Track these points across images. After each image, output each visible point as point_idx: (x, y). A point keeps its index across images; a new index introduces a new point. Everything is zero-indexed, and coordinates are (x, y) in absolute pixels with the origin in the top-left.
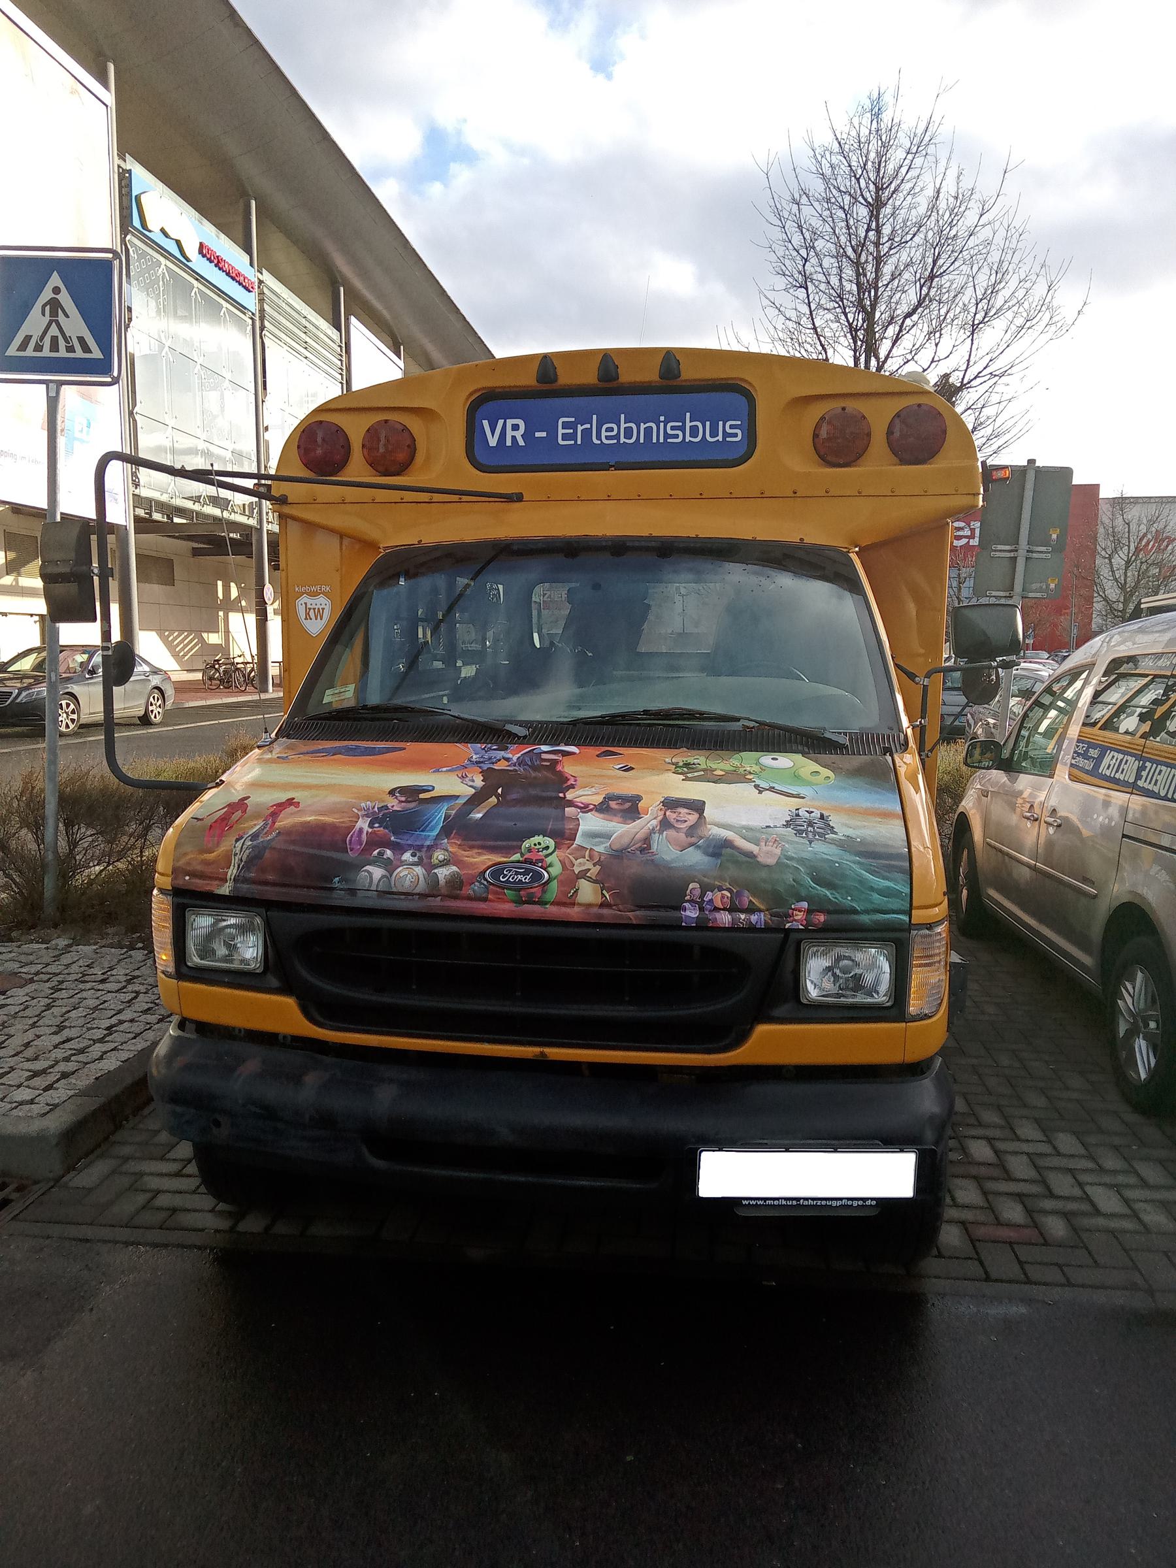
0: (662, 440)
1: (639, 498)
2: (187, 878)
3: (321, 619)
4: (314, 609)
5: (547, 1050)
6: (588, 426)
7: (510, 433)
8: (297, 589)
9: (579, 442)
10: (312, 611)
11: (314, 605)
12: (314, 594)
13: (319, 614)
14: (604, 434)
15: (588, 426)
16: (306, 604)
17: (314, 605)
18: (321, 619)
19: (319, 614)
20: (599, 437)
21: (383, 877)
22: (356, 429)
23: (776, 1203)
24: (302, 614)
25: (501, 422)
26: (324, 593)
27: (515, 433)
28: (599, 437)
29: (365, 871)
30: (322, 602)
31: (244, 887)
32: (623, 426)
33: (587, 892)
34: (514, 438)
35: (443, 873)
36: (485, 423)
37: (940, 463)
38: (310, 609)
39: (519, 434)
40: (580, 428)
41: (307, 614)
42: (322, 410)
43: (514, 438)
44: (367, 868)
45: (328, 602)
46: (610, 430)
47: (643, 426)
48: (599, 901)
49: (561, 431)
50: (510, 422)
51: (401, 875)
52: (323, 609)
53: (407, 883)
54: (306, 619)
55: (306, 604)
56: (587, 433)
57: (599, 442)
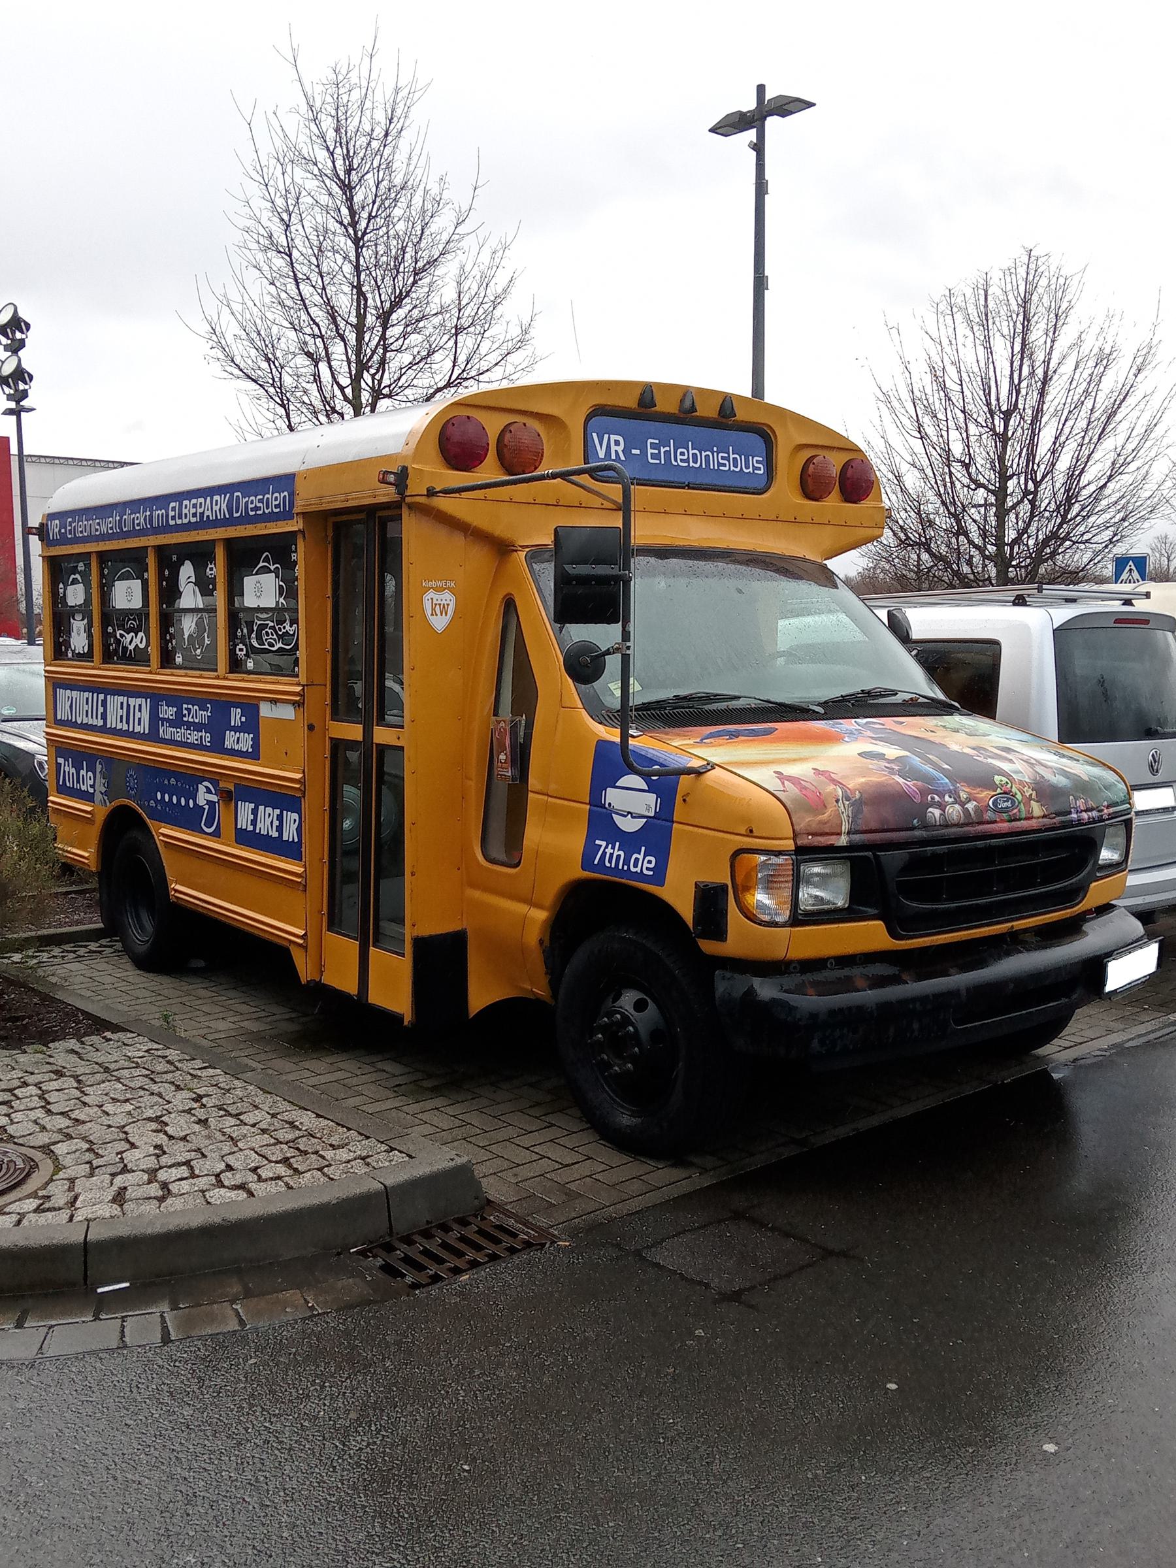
0: (716, 468)
1: (705, 515)
2: (810, 837)
3: (446, 615)
4: (440, 605)
5: (1015, 923)
6: (668, 449)
7: (613, 448)
8: (424, 584)
9: (663, 462)
10: (438, 606)
11: (439, 600)
12: (439, 590)
13: (444, 610)
14: (679, 457)
15: (668, 449)
16: (432, 599)
17: (439, 600)
18: (446, 615)
19: (444, 610)
20: (676, 461)
21: (941, 815)
22: (493, 425)
23: (1125, 988)
24: (429, 611)
25: (606, 436)
26: (448, 589)
27: (617, 448)
28: (676, 461)
29: (930, 812)
30: (447, 598)
31: (857, 838)
32: (691, 452)
33: (1037, 809)
34: (616, 452)
35: (970, 806)
36: (595, 435)
37: (867, 503)
38: (436, 604)
39: (620, 449)
40: (663, 450)
41: (433, 609)
42: (457, 404)
43: (616, 452)
44: (930, 810)
45: (453, 598)
46: (682, 454)
47: (704, 454)
48: (1042, 814)
49: (650, 451)
50: (613, 438)
51: (950, 812)
52: (448, 605)
53: (955, 818)
54: (432, 615)
55: (432, 599)
56: (667, 453)
57: (676, 464)
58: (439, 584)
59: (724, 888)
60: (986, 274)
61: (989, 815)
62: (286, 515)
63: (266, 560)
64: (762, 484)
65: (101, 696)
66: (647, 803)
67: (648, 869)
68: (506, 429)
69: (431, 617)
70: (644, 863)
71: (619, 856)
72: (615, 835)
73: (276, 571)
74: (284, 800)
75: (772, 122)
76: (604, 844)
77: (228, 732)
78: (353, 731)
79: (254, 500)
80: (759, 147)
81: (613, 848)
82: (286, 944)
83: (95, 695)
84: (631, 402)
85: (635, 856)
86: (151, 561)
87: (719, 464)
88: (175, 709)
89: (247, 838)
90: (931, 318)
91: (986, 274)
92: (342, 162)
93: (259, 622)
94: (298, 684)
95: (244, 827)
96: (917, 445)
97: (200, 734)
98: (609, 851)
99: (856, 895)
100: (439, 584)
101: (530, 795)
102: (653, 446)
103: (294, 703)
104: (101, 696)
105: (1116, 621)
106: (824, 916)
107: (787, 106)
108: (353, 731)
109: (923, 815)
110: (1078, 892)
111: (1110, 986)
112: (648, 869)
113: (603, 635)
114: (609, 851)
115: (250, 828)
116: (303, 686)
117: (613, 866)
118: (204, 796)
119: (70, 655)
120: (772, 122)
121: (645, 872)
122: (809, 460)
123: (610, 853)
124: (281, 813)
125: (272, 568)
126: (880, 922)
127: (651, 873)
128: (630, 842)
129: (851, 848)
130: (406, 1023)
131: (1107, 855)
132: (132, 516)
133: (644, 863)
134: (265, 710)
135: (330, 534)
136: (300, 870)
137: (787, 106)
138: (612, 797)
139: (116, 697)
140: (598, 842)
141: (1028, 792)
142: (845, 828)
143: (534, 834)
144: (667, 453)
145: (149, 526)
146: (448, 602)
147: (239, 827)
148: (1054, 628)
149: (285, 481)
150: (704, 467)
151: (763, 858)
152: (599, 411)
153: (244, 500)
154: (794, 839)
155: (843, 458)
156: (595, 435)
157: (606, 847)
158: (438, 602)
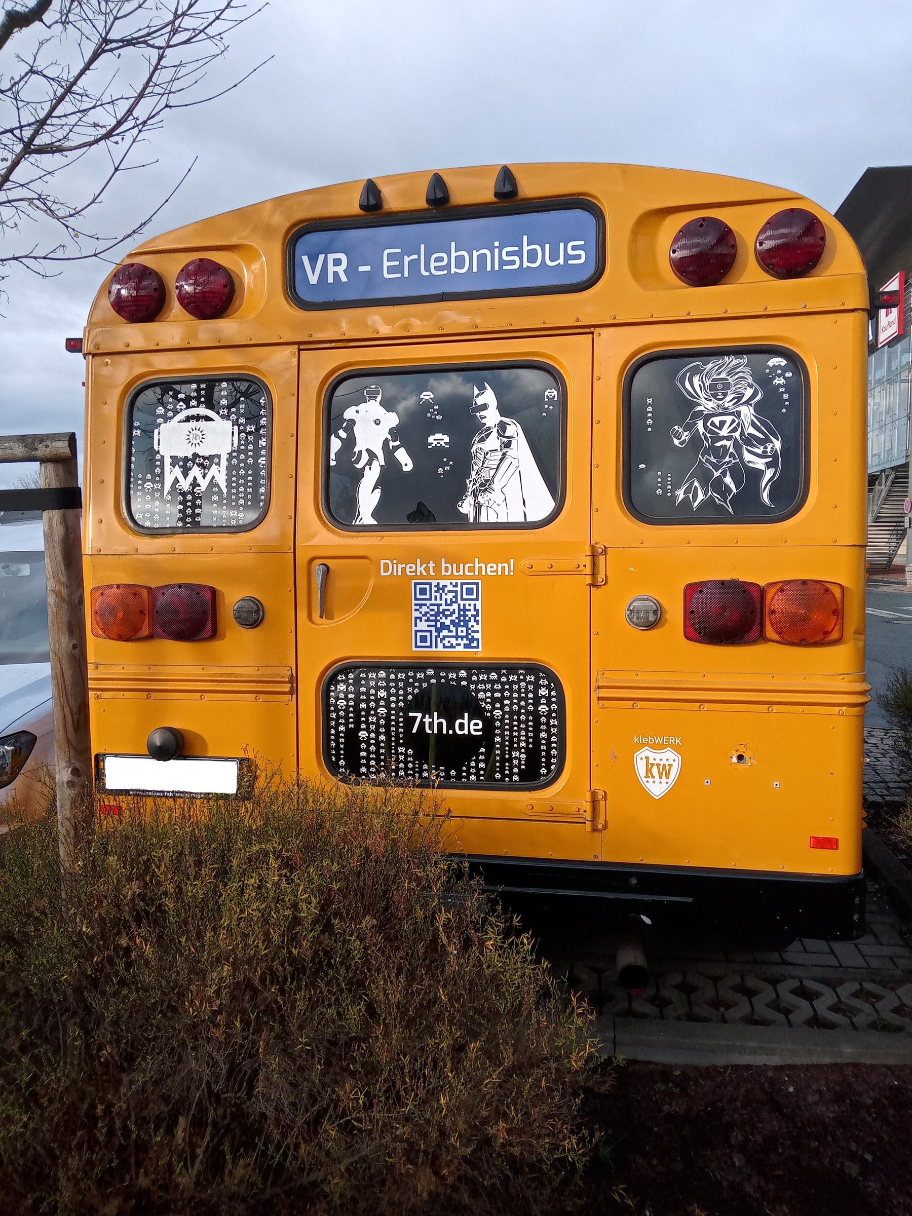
0: (497, 268)
6: (416, 257)
7: (331, 269)
13: (664, 771)
14: (433, 264)
15: (416, 257)
19: (664, 771)
26: (672, 746)
27: (337, 269)
28: (427, 268)
30: (669, 757)
36: (305, 259)
38: (652, 765)
39: (341, 269)
40: (407, 259)
43: (336, 274)
49: (386, 264)
50: (331, 257)
52: (670, 766)
55: (647, 758)
56: (414, 264)
57: (428, 274)
58: (658, 740)
67: (475, 730)
69: (645, 780)
71: (440, 724)
76: (419, 715)
81: (431, 717)
87: (502, 262)
98: (427, 720)
100: (658, 740)
102: (391, 257)
112: (475, 730)
117: (436, 732)
121: (473, 733)
127: (480, 733)
144: (414, 264)
146: (671, 762)
150: (475, 270)
156: (305, 259)
157: (423, 717)
158: (655, 762)
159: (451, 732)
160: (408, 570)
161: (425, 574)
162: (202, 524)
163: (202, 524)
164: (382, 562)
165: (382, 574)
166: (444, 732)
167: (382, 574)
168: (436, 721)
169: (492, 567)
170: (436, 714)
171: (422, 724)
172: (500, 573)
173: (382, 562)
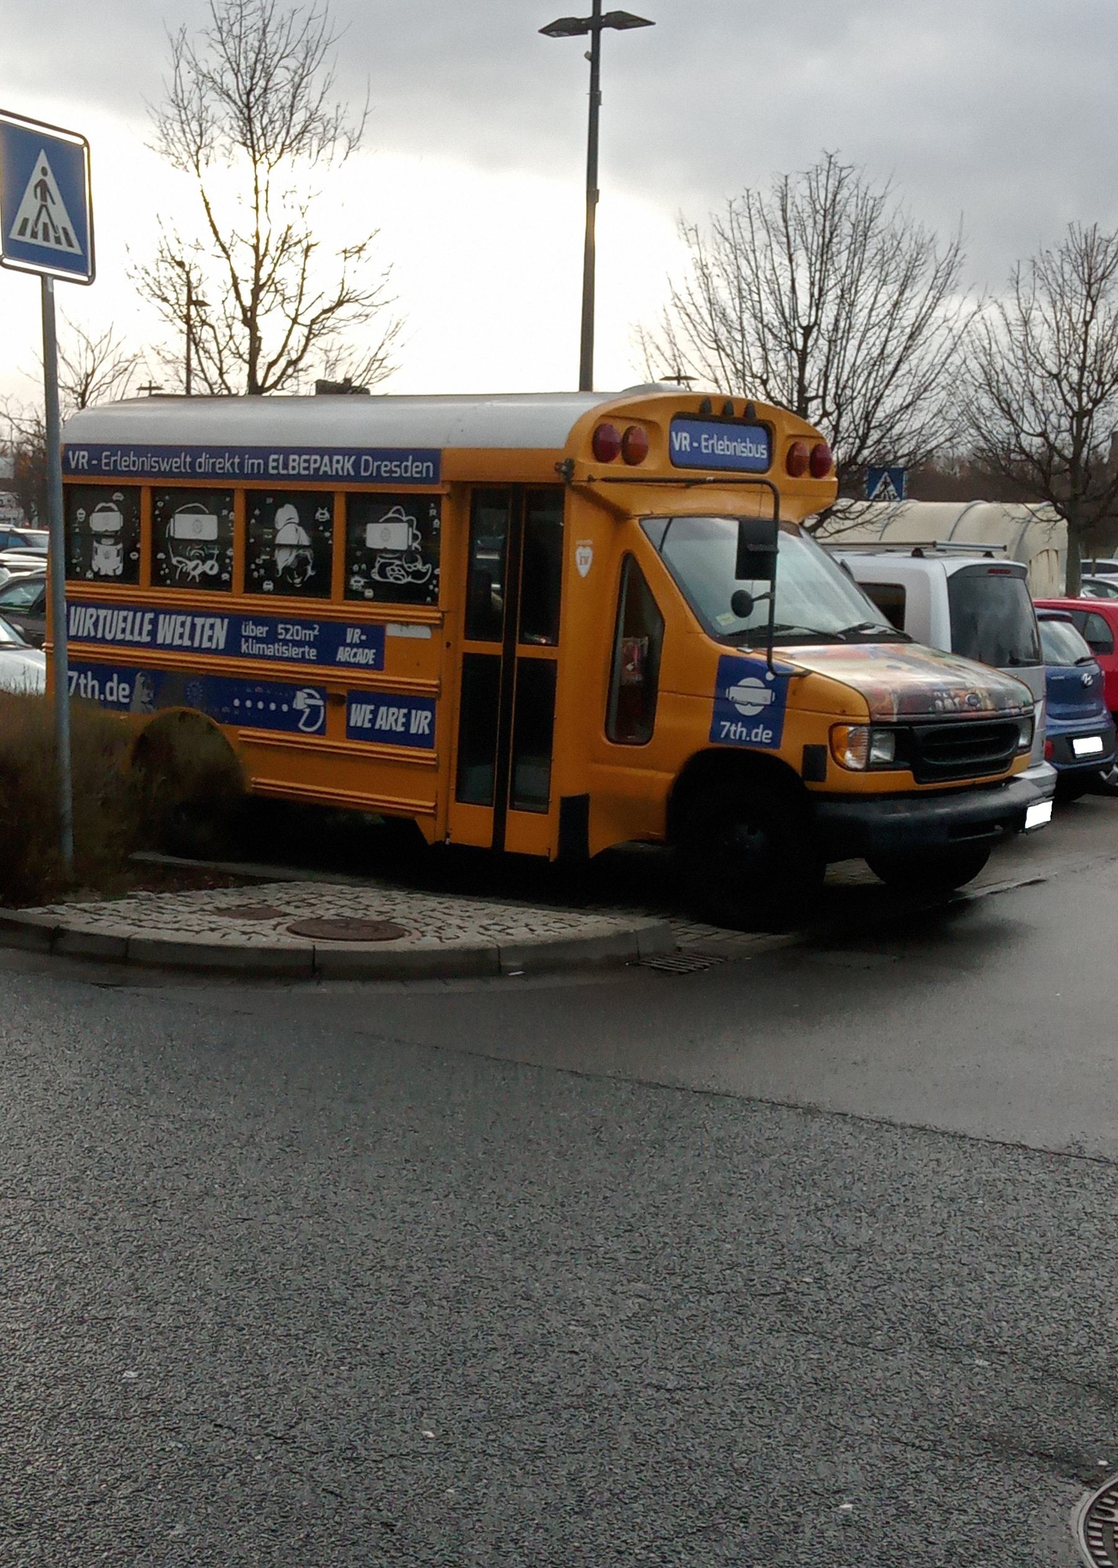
22: (620, 428)
24: (578, 561)
35: (957, 700)
59: (824, 748)
60: (786, 177)
61: (966, 707)
62: (435, 480)
63: (397, 511)
64: (763, 466)
65: (149, 616)
66: (765, 696)
68: (629, 431)
70: (762, 735)
71: (742, 732)
72: (736, 718)
73: (410, 523)
74: (422, 702)
75: (607, 33)
76: (728, 724)
77: (341, 649)
78: (494, 648)
79: (386, 466)
80: (594, 57)
82: (410, 815)
83: (139, 615)
84: (694, 409)
85: (755, 731)
86: (239, 501)
88: (266, 629)
89: (356, 733)
90: (724, 215)
91: (786, 177)
92: (272, 97)
93: (382, 561)
94: (439, 611)
95: (359, 724)
96: (713, 356)
97: (302, 650)
98: (82, 681)
99: (897, 756)
101: (660, 694)
103: (430, 625)
104: (149, 616)
105: (991, 571)
106: (881, 766)
107: (623, 21)
108: (494, 648)
109: (934, 705)
110: (1006, 763)
111: (1028, 825)
113: (759, 587)
114: (733, 728)
115: (367, 725)
116: (443, 613)
118: (301, 701)
119: (89, 575)
120: (607, 33)
122: (793, 447)
123: (734, 730)
124: (409, 713)
125: (404, 519)
126: (910, 772)
128: (751, 722)
129: (898, 723)
130: (551, 860)
131: (1022, 741)
132: (212, 461)
133: (762, 735)
134: (392, 631)
135: (469, 497)
136: (434, 756)
137: (623, 21)
138: (734, 693)
139: (174, 617)
140: (723, 723)
141: (985, 694)
142: (895, 711)
143: (664, 719)
145: (237, 471)
147: (352, 724)
148: (949, 574)
149: (431, 455)
151: (851, 728)
152: (680, 416)
153: (376, 464)
154: (870, 716)
155: (814, 442)
157: (79, 677)
159: (102, 697)
160: (383, 469)
161: (352, 473)
162: (373, 393)
163: (373, 393)
164: (364, 458)
165: (363, 474)
166: (96, 697)
167: (363, 474)
168: (739, 730)
169: (417, 467)
170: (89, 674)
171: (729, 731)
172: (424, 475)
173: (364, 458)
